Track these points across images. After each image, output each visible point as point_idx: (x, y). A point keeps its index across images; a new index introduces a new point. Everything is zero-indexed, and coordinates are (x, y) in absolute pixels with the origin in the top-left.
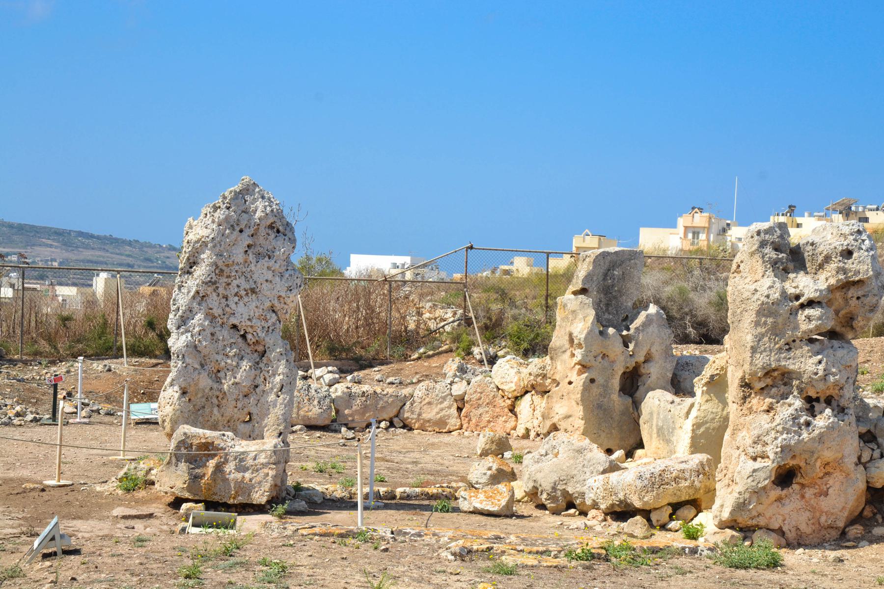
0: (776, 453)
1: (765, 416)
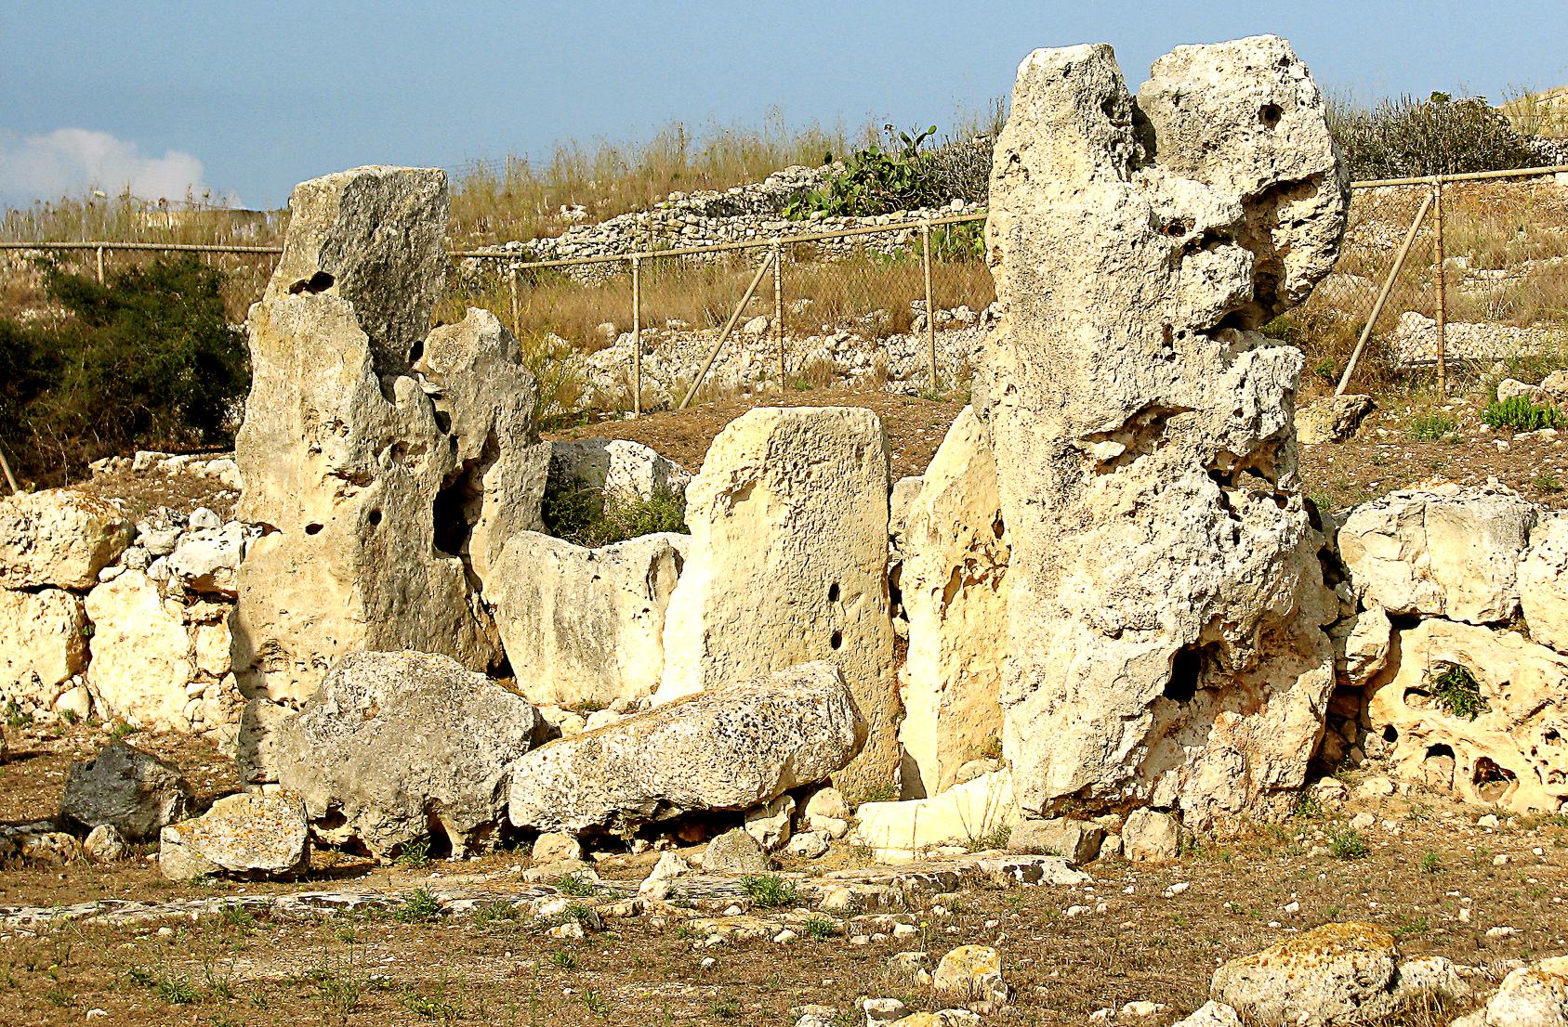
0: (1179, 614)
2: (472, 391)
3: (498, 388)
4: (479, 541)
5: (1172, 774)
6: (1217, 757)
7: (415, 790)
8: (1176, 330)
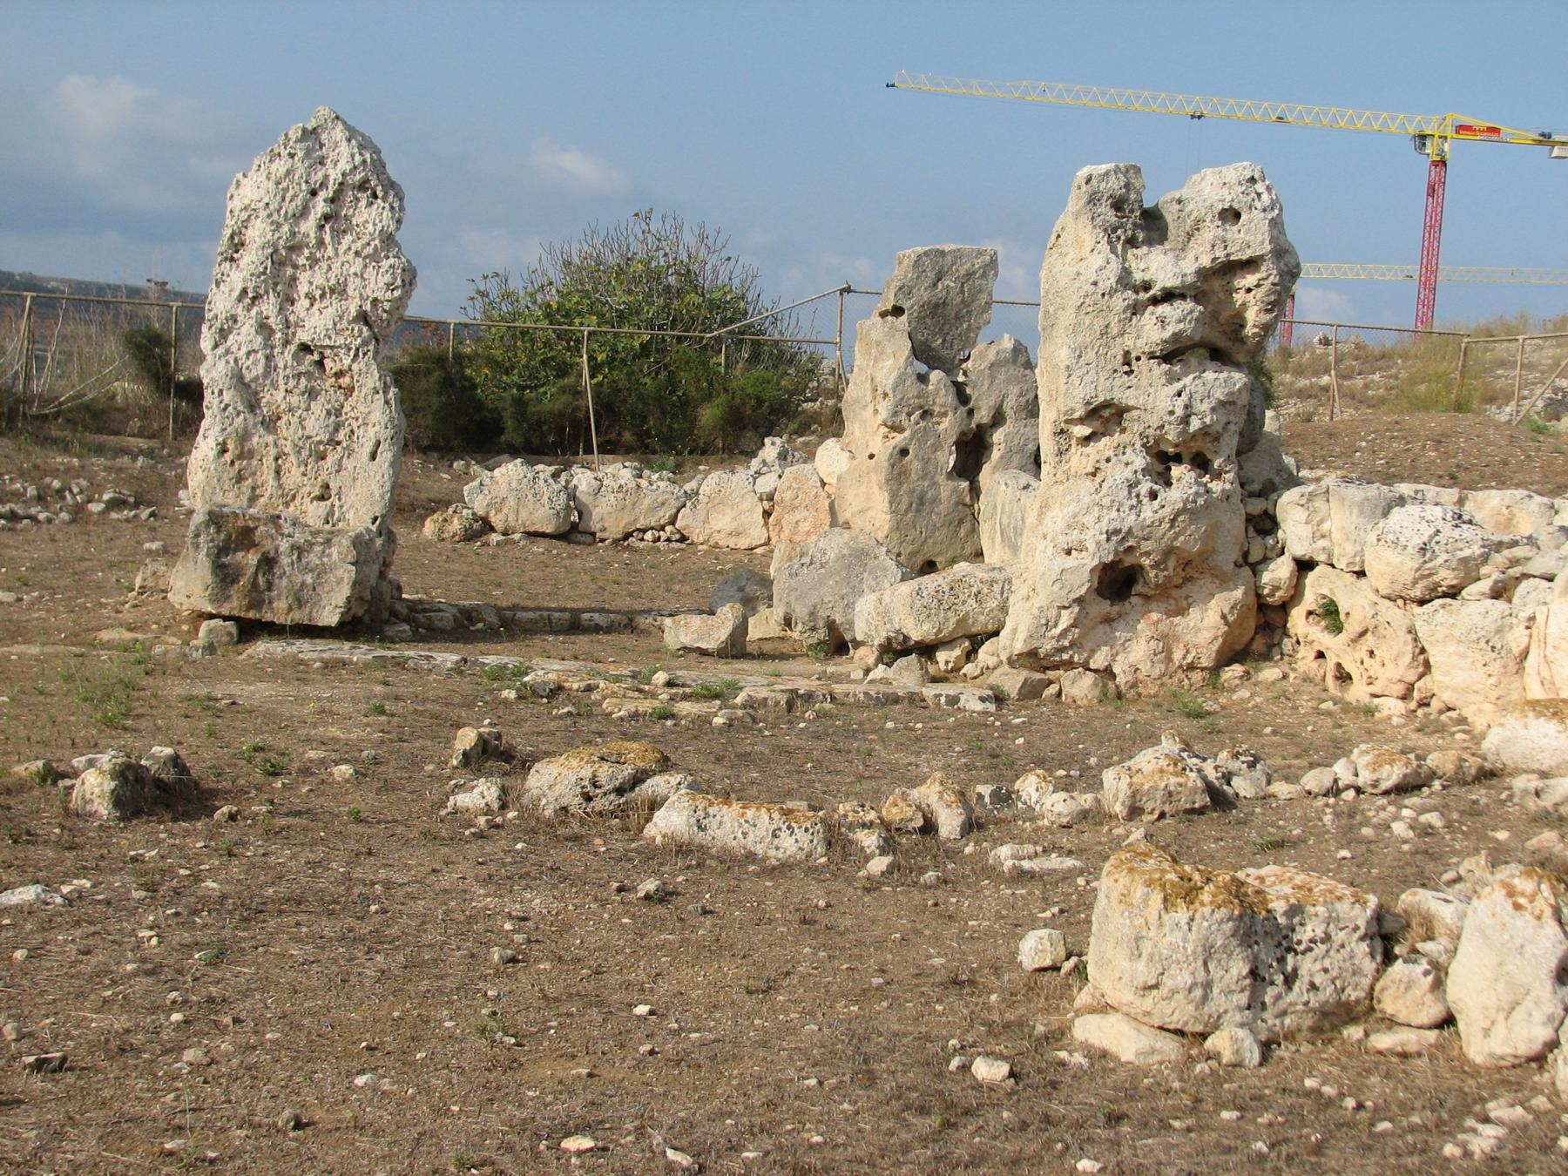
1: (1088, 483)
2: (987, 383)
3: (1008, 382)
4: (985, 476)
5: (1105, 649)
6: (1143, 641)
7: (823, 613)
8: (1133, 355)
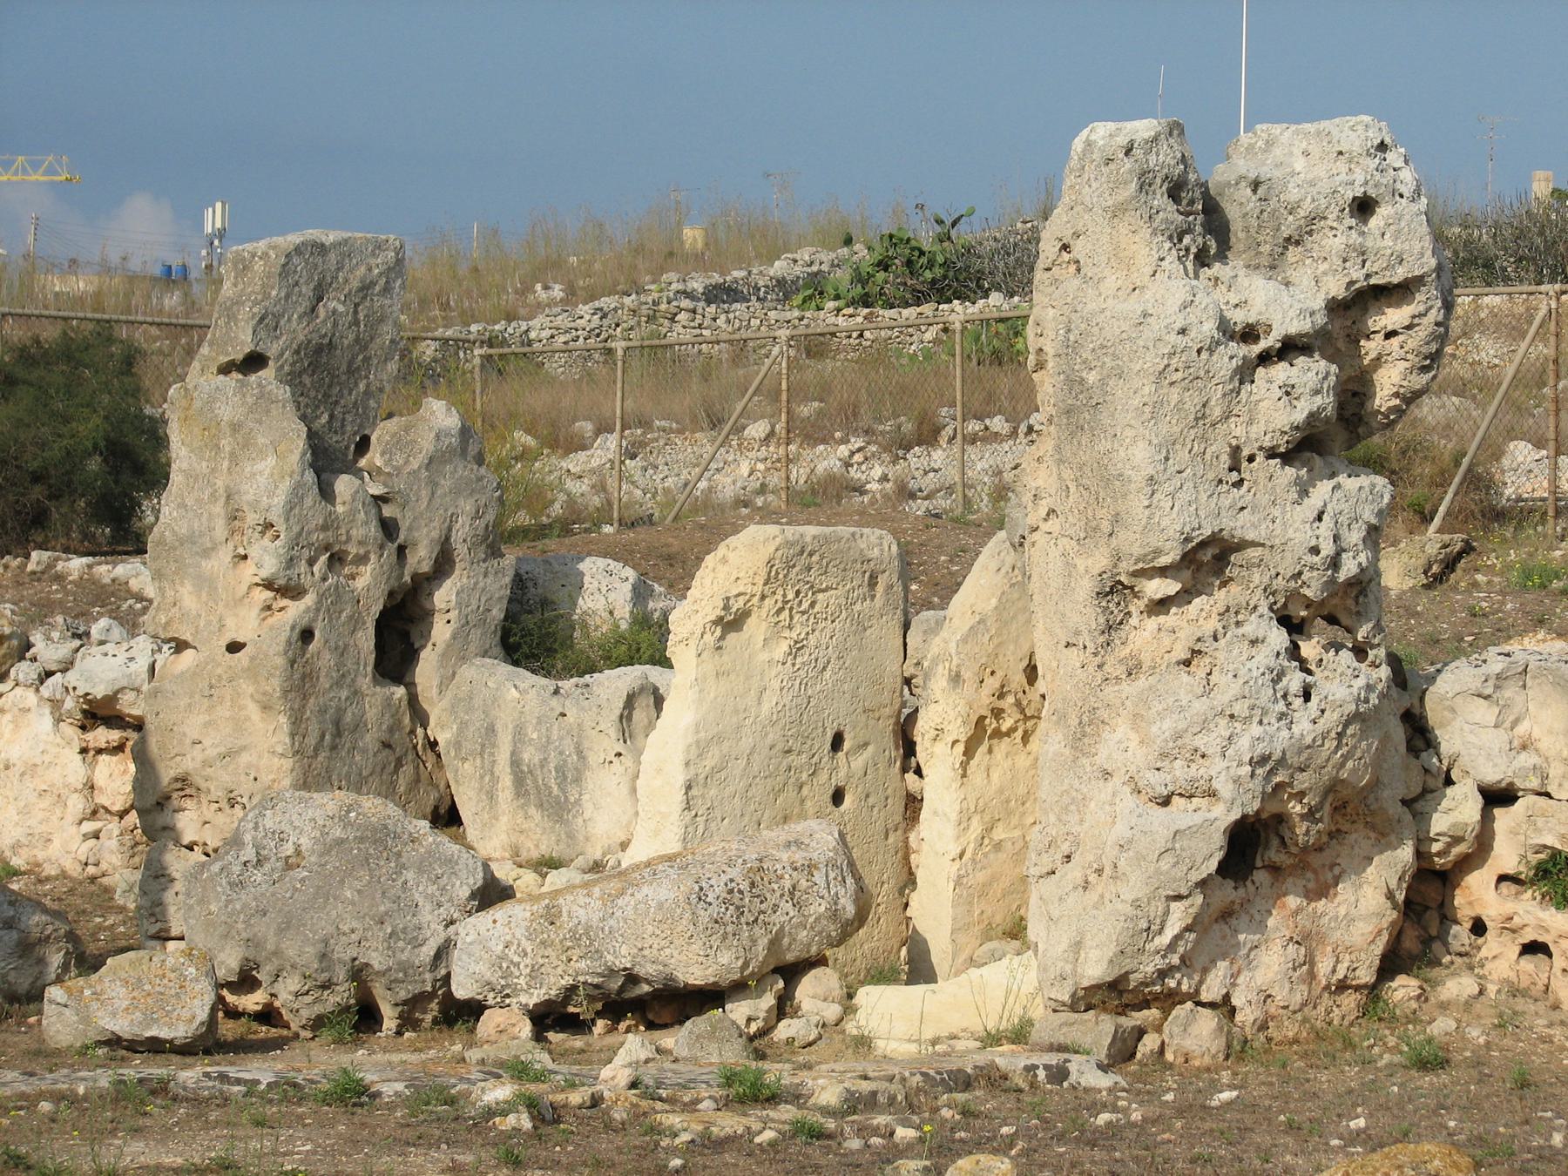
0: (1237, 781)
3: (456, 492)
4: (427, 669)
5: (1222, 966)
6: (1277, 946)
7: (343, 953)
8: (1246, 453)
